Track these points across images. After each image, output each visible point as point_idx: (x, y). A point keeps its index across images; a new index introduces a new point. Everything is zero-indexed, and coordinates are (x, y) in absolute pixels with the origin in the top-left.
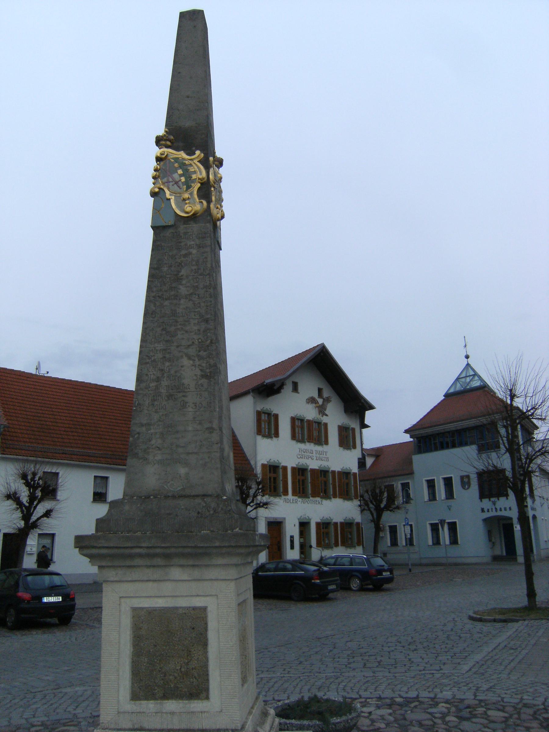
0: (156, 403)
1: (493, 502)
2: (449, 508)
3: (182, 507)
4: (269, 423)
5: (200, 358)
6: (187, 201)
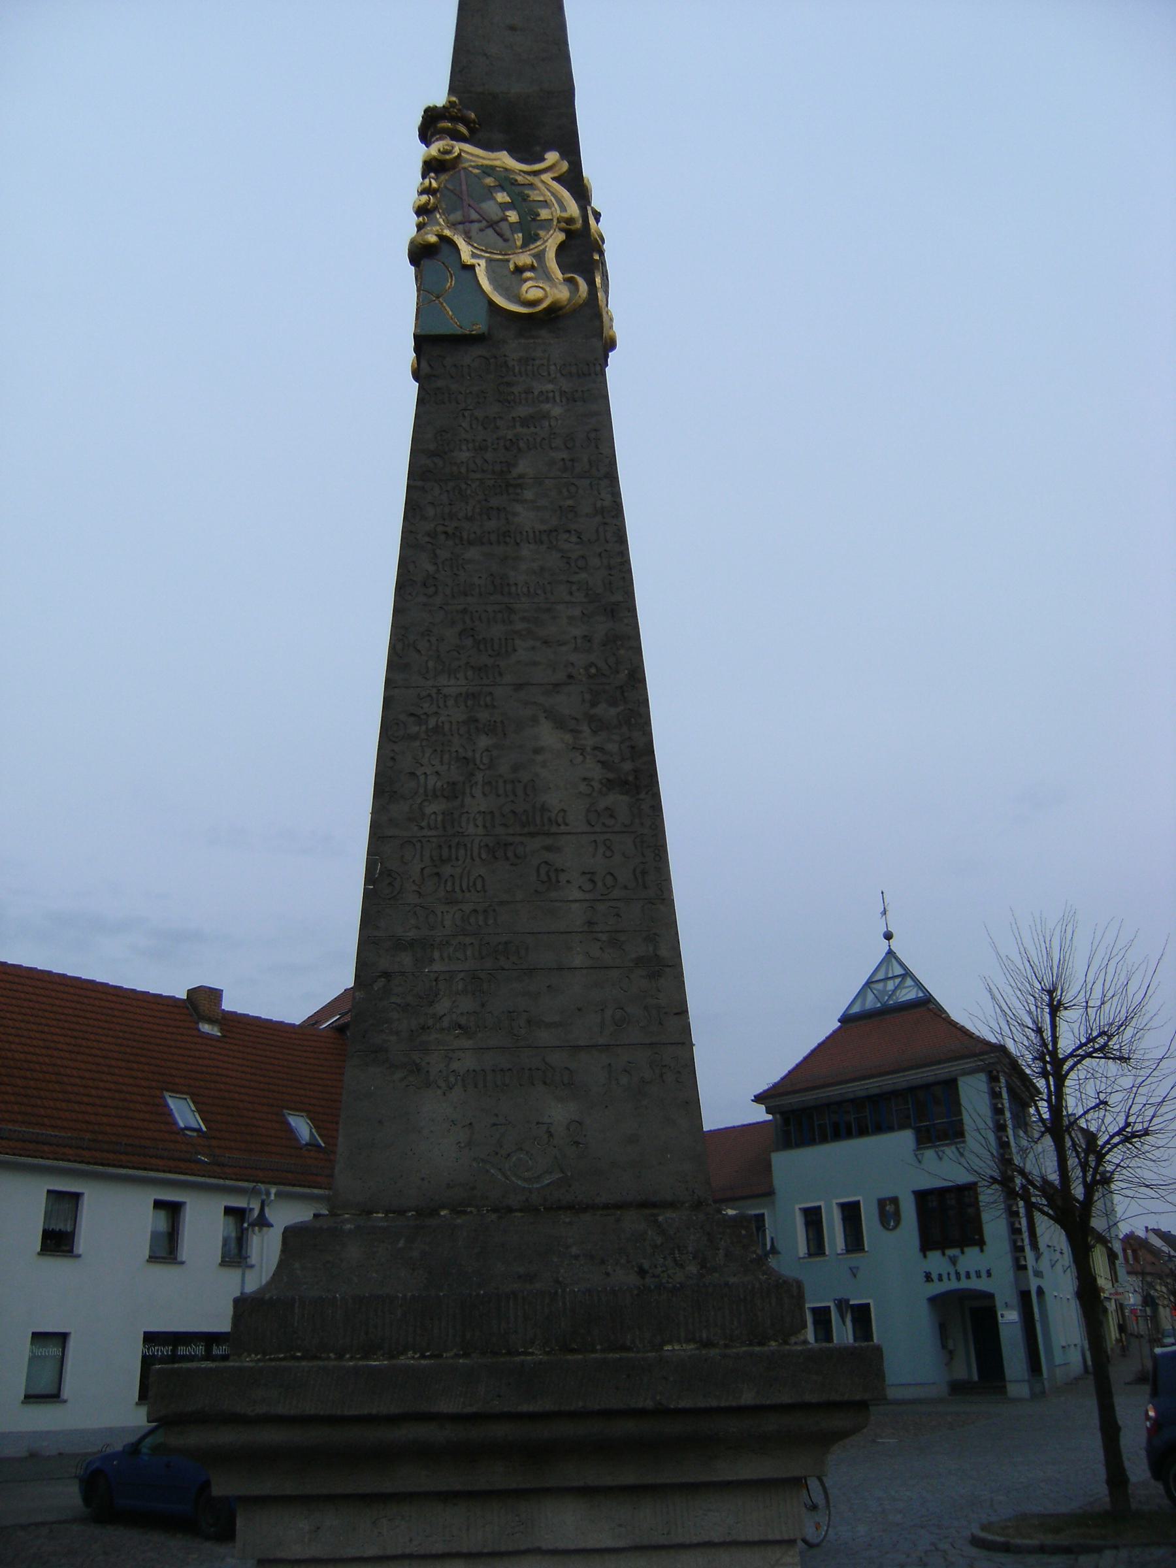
0: (447, 870)
1: (950, 1258)
2: (854, 1272)
3: (574, 1250)
5: (599, 725)
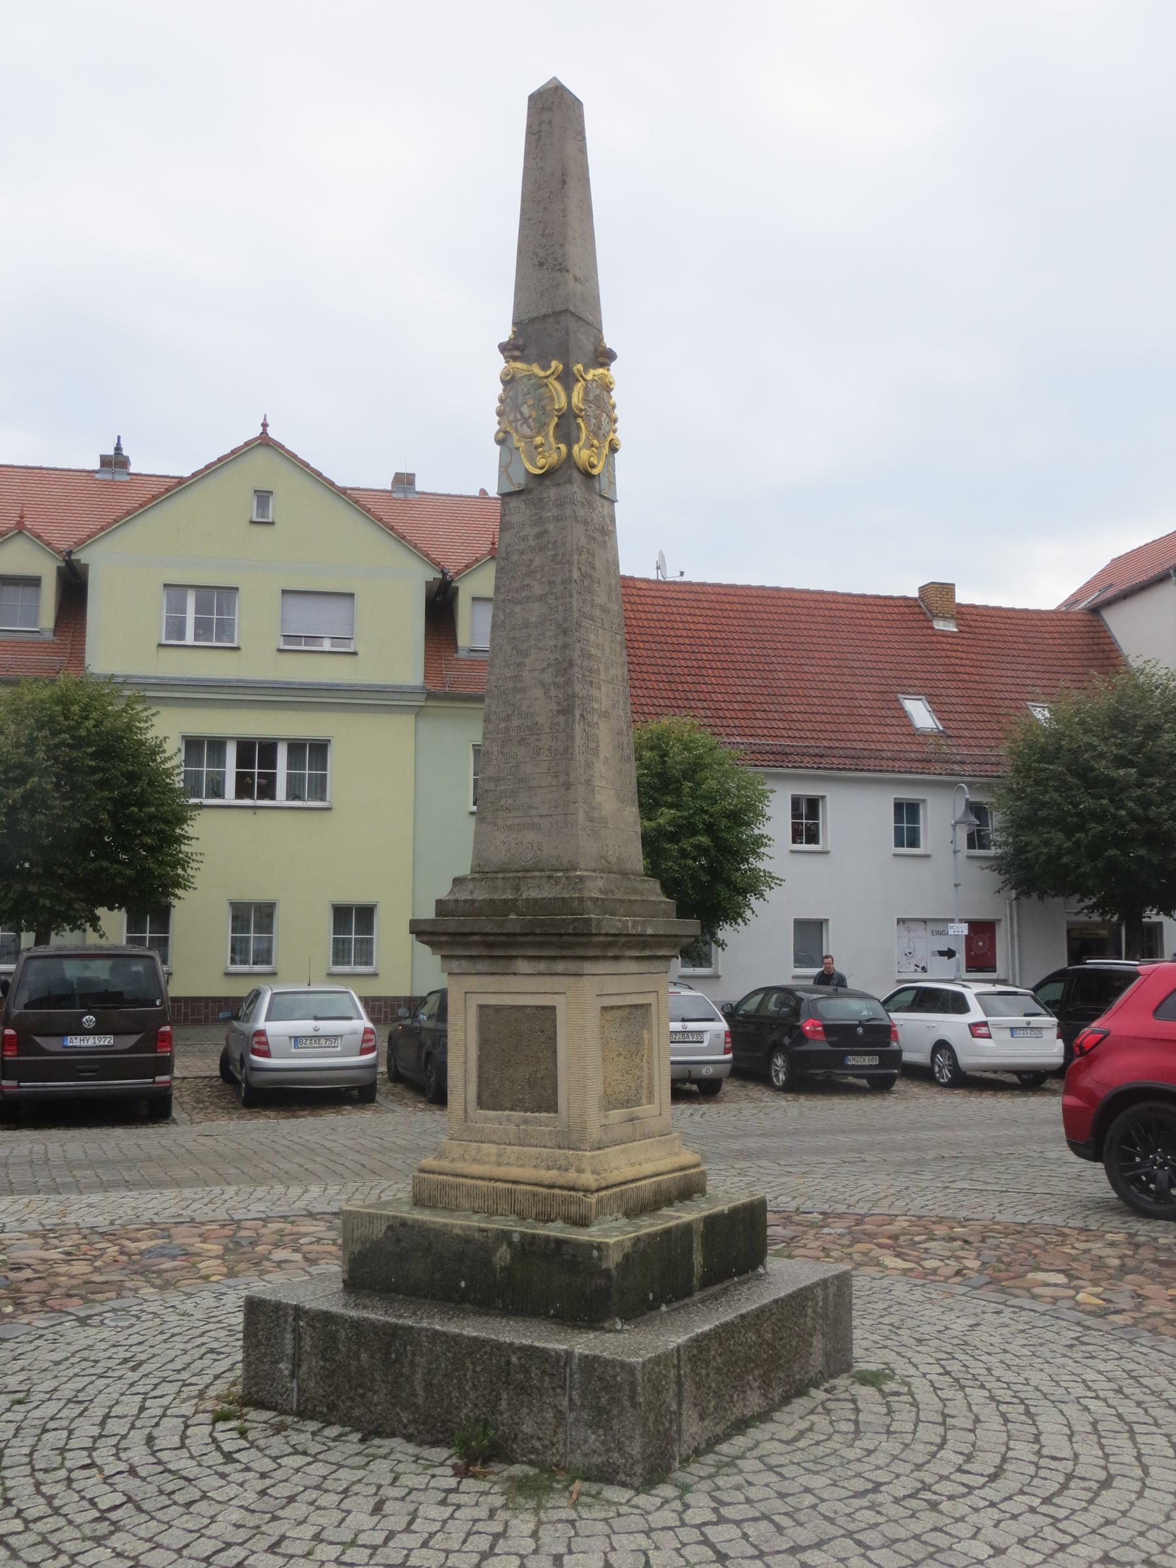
5: (557, 685)
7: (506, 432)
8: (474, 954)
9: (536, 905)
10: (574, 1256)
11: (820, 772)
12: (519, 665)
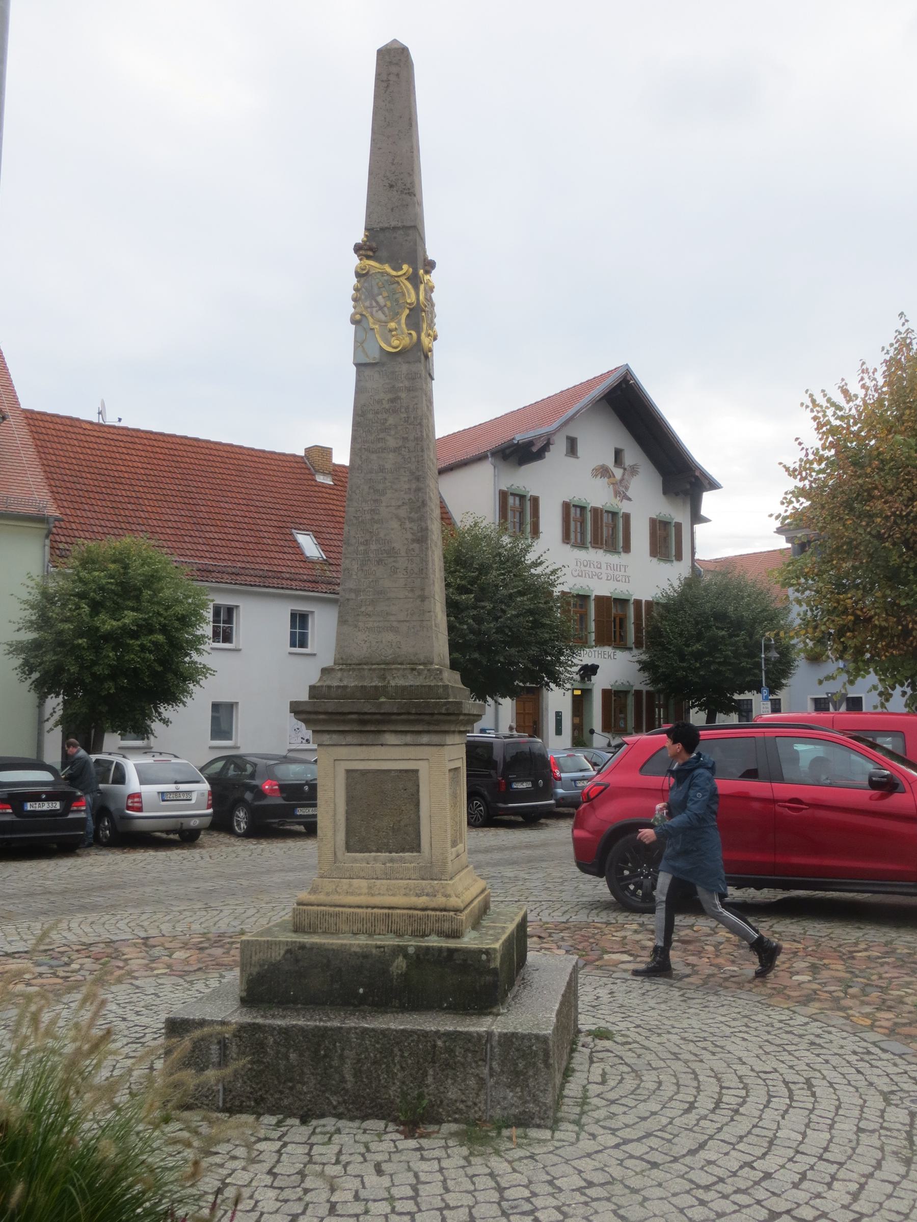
0: (365, 568)
4: (522, 513)
5: (411, 520)
6: (394, 333)
7: (362, 315)
8: (347, 729)
9: (403, 691)
10: (465, 960)
11: (237, 587)
12: (376, 501)
